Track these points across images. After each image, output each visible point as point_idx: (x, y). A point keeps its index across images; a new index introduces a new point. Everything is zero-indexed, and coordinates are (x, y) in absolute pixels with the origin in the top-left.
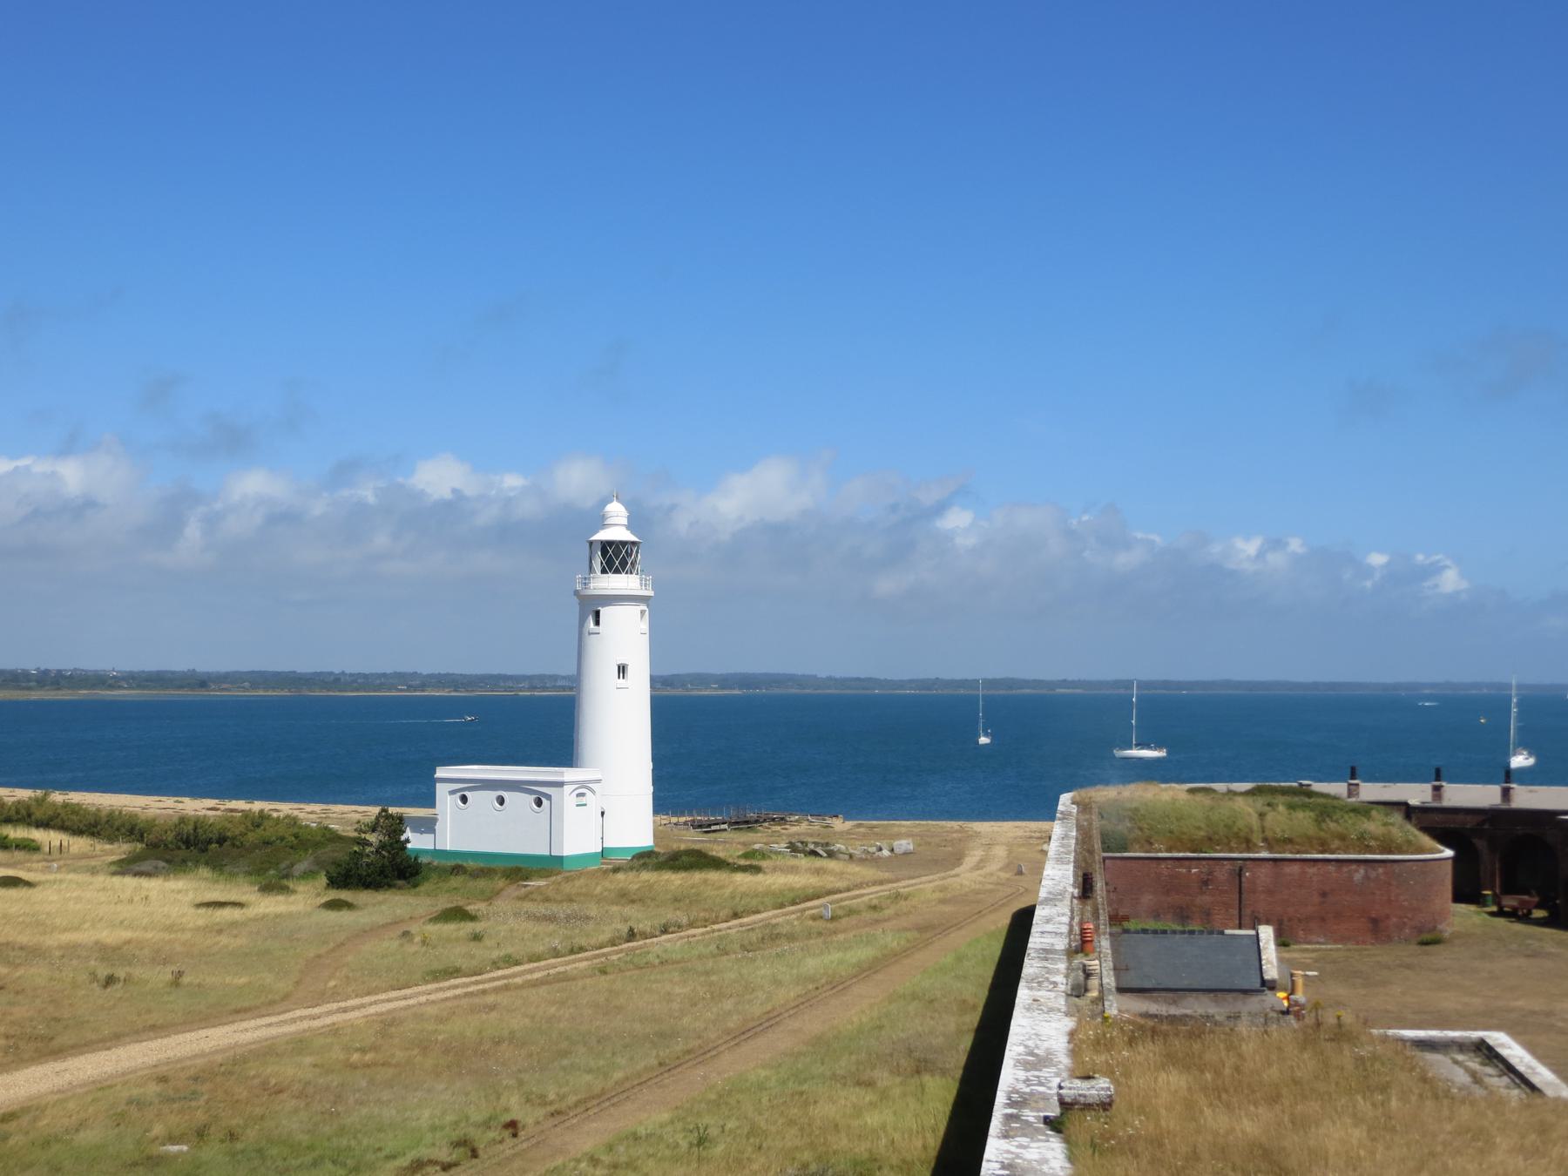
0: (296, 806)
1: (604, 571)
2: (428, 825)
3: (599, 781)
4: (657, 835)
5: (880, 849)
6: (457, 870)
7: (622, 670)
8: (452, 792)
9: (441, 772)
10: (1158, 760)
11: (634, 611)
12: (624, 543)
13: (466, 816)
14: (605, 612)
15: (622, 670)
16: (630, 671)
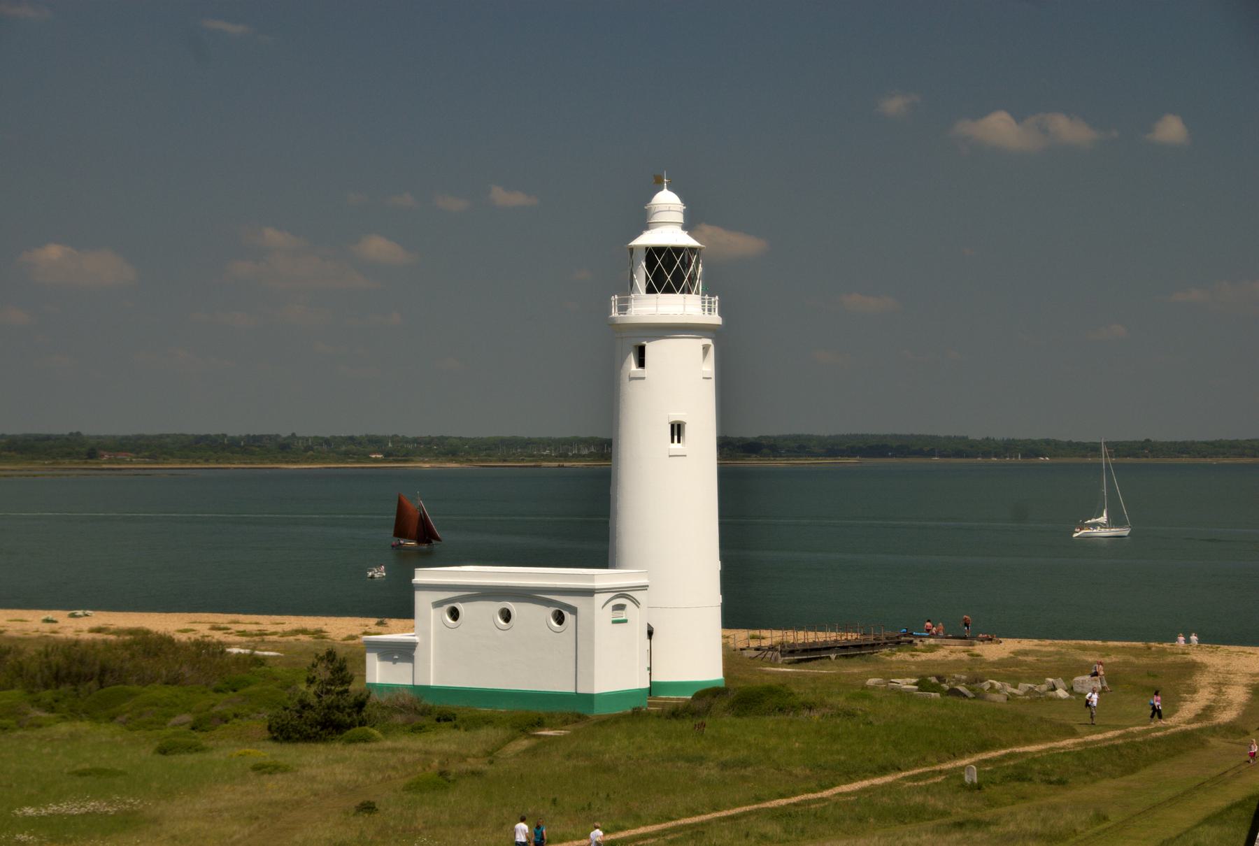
0: (222, 619)
1: (650, 290)
2: (405, 652)
3: (644, 588)
4: (731, 658)
5: (1054, 689)
6: (445, 718)
7: (677, 430)
8: (438, 604)
9: (423, 576)
10: (565, 736)
11: (694, 345)
12: (678, 250)
13: (461, 636)
14: (652, 349)
15: (677, 430)
16: (688, 431)
